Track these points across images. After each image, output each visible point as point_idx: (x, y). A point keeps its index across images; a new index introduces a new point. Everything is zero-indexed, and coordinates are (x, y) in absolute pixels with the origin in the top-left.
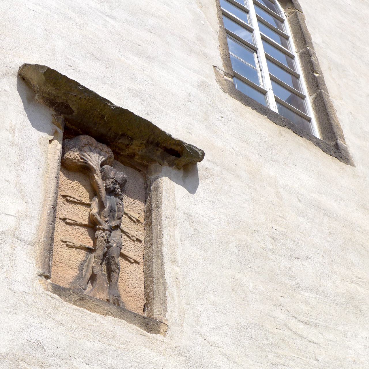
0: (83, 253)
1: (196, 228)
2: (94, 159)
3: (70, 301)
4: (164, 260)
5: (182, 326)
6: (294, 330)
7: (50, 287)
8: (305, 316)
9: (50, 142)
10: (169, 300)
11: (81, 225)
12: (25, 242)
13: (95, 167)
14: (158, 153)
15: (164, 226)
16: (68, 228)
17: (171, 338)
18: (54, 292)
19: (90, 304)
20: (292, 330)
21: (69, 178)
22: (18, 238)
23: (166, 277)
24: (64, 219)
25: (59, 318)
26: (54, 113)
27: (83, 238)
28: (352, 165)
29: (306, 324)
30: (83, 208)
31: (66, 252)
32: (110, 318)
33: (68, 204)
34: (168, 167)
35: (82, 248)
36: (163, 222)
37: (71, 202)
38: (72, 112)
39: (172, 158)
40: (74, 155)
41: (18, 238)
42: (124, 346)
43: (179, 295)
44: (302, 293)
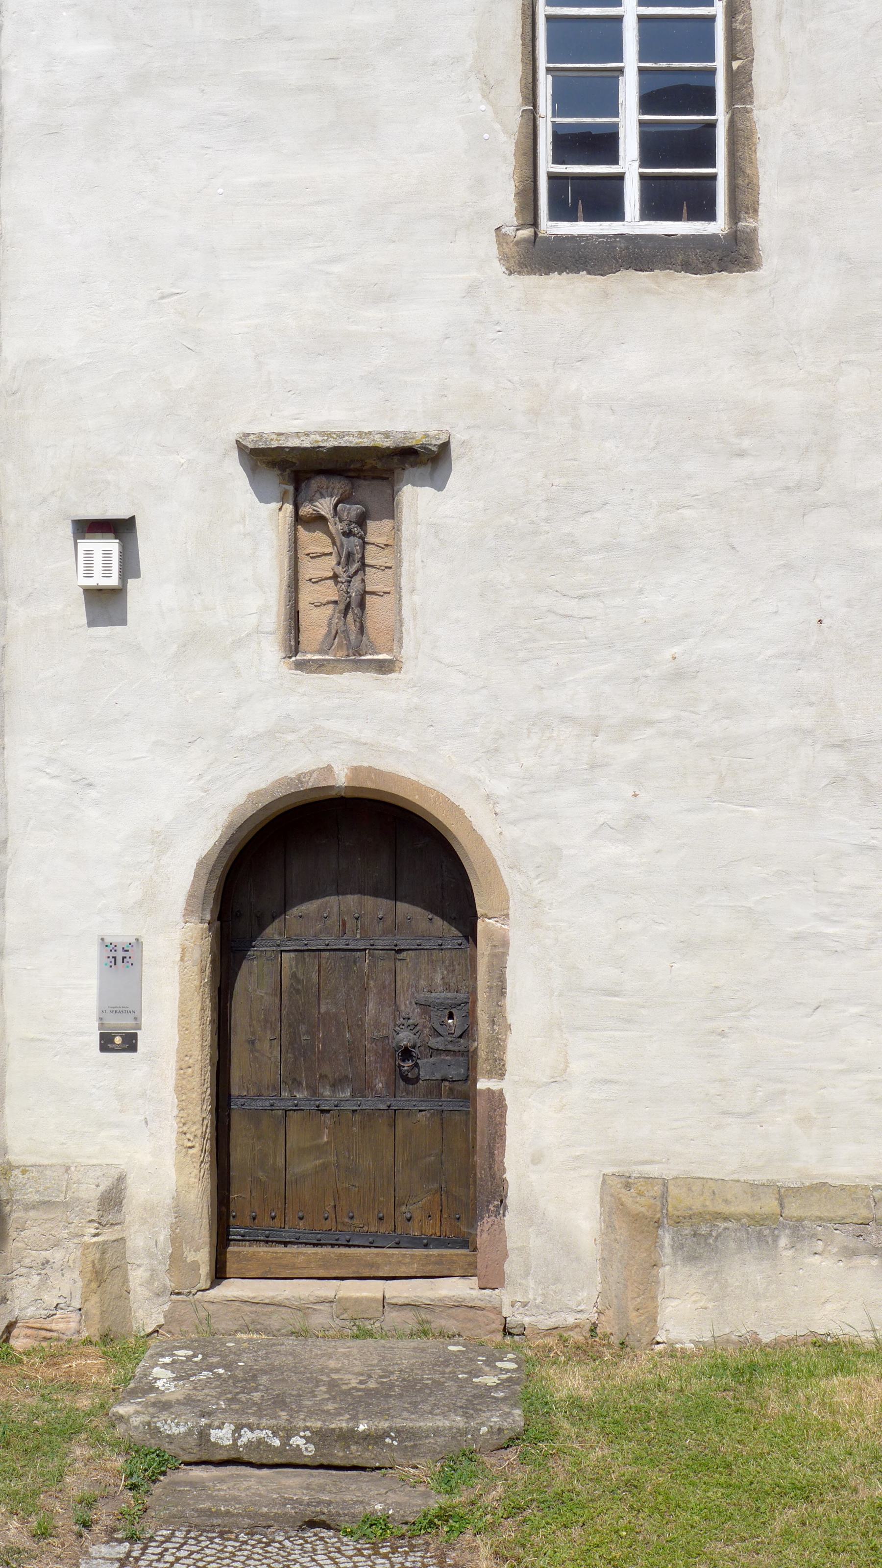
0: (331, 606)
1: (441, 537)
2: (324, 506)
3: (311, 672)
4: (403, 594)
5: (417, 658)
6: (560, 612)
7: (293, 666)
8: (581, 589)
9: (280, 509)
10: (405, 635)
11: (327, 579)
12: (268, 633)
13: (327, 516)
14: (396, 461)
15: (403, 552)
16: (316, 586)
17: (406, 673)
18: (296, 669)
19: (329, 668)
20: (556, 614)
21: (310, 531)
22: (261, 632)
23: (403, 612)
24: (310, 580)
25: (301, 690)
26: (279, 472)
27: (330, 591)
28: (121, 1179)
29: (580, 598)
30: (328, 557)
31: (316, 613)
32: (346, 674)
33: (313, 560)
34: (411, 469)
35: (329, 603)
36: (403, 548)
37: (314, 557)
38: (294, 464)
39: (412, 459)
40: (306, 510)
41: (261, 632)
42: (359, 696)
43: (415, 628)
44: (584, 559)
